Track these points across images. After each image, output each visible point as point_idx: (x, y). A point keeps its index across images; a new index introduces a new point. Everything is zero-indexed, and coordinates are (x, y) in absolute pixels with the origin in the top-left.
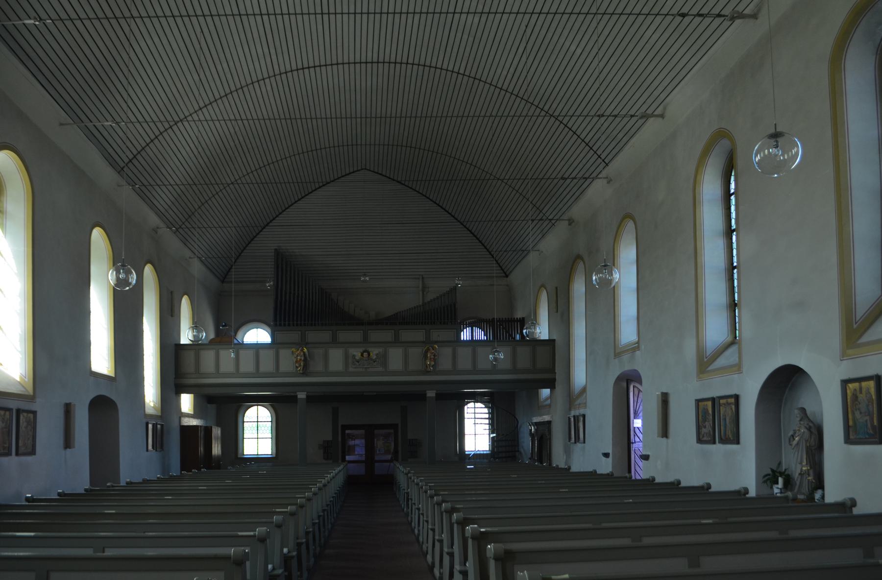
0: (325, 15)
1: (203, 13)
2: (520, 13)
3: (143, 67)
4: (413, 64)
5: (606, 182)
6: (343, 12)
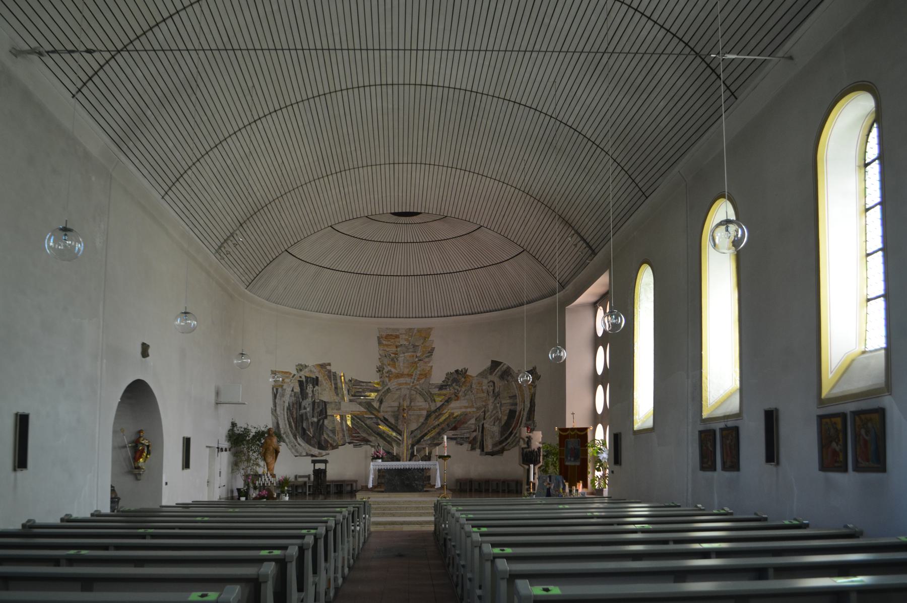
0: (414, 51)
1: (187, 48)
2: (542, 51)
3: (158, 57)
4: (164, 20)
5: (239, 487)
6: (410, 51)
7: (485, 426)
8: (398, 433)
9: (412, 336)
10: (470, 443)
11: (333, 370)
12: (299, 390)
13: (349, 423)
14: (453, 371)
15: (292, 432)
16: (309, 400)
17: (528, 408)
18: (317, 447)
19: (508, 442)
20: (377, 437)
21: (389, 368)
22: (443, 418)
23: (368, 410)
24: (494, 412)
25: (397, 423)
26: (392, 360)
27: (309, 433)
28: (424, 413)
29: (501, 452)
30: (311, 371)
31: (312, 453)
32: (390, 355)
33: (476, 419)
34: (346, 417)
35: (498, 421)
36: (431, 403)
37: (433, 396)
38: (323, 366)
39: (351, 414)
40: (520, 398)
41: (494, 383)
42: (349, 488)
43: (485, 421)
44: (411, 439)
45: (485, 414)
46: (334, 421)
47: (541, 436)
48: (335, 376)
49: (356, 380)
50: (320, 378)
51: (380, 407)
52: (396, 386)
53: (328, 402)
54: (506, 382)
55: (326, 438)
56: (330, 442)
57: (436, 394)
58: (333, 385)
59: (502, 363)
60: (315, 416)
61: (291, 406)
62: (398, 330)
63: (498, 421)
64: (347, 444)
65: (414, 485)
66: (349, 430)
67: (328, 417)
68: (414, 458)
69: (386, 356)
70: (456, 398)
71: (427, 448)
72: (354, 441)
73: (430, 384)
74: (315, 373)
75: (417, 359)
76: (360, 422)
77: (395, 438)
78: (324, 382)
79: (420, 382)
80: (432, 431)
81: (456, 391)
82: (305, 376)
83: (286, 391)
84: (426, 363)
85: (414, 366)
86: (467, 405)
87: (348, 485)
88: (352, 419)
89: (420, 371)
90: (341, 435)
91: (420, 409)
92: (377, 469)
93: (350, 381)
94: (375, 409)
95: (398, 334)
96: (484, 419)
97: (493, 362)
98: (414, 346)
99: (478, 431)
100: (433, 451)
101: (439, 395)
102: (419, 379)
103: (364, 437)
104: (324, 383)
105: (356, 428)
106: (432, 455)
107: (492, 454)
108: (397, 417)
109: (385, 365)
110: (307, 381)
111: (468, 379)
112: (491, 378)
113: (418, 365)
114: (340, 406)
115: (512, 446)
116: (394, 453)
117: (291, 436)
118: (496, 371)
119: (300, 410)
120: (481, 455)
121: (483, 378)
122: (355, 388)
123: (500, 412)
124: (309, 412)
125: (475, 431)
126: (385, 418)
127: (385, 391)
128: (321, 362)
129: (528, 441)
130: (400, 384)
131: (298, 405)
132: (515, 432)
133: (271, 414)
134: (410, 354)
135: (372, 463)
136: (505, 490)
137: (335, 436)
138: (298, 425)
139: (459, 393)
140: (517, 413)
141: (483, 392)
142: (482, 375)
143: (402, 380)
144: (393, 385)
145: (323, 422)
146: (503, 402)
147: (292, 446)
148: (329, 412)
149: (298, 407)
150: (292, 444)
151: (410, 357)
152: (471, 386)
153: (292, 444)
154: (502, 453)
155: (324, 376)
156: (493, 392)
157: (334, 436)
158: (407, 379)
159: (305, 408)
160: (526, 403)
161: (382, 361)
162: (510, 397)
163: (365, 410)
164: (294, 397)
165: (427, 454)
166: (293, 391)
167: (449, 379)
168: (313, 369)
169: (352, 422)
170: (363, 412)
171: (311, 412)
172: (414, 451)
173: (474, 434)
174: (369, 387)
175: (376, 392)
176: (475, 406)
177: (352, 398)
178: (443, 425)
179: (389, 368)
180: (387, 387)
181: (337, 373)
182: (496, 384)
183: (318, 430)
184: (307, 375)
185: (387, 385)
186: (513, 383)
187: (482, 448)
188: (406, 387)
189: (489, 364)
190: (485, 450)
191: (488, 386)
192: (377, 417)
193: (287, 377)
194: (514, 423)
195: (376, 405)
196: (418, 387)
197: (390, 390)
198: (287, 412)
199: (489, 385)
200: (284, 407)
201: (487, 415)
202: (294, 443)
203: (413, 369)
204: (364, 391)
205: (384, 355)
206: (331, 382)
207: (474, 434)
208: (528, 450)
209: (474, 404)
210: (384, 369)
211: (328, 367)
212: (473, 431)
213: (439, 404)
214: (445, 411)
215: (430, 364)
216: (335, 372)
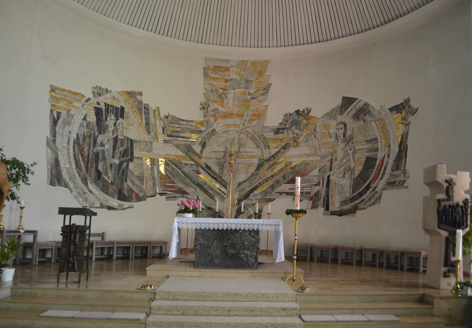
7: (332, 178)
8: (222, 184)
9: (244, 70)
10: (311, 199)
11: (145, 102)
12: (95, 120)
13: (162, 168)
14: (292, 111)
15: (80, 175)
16: (109, 135)
17: (395, 154)
18: (116, 196)
19: (362, 198)
20: (196, 189)
21: (216, 106)
22: (278, 168)
23: (187, 155)
24: (345, 161)
25: (222, 173)
26: (220, 96)
27: (107, 179)
28: (256, 161)
29: (353, 210)
30: (114, 98)
31: (108, 204)
32: (218, 90)
33: (319, 170)
34: (158, 162)
35: (350, 173)
36: (264, 150)
37: (267, 142)
38: (131, 94)
39: (165, 158)
40: (383, 141)
41: (345, 125)
42: (157, 251)
43: (331, 173)
44: (238, 193)
45: (331, 164)
46: (143, 164)
47: (469, 180)
48: (148, 109)
49: (175, 117)
50: (126, 109)
51: (202, 152)
52: (223, 128)
53: (136, 141)
54: (362, 123)
55: (131, 186)
56: (136, 191)
57: (270, 139)
58: (144, 120)
59: (357, 99)
60: (116, 156)
61: (81, 139)
62: (228, 61)
63: (350, 173)
64: (158, 195)
65: (242, 256)
66: (161, 178)
67: (135, 159)
68: (241, 216)
69: (212, 91)
70: (296, 144)
71: (257, 204)
72: (167, 192)
73: (264, 127)
74: (120, 101)
75: (249, 97)
76: (176, 168)
77: (218, 190)
78: (131, 114)
79: (253, 123)
80: (264, 183)
81: (295, 135)
82: (105, 104)
83: (75, 118)
84: (260, 101)
85: (246, 105)
86: (308, 152)
87: (154, 247)
88: (166, 164)
89: (253, 111)
90: (150, 183)
91: (251, 157)
92: (194, 228)
93: (167, 117)
94: (196, 154)
95: (228, 66)
96: (331, 170)
97: (344, 99)
98: (247, 81)
99: (321, 185)
100: (264, 208)
101: (275, 140)
102: (251, 121)
103: (180, 188)
104: (132, 116)
105: (171, 177)
106: (262, 213)
107: (340, 214)
108: (223, 166)
109: (211, 101)
110: (107, 110)
111: (311, 121)
112: (341, 118)
113: (251, 104)
114: (152, 147)
115: (369, 204)
116: (216, 209)
117: (79, 180)
118: (349, 110)
119: (94, 147)
120: (324, 214)
121: (331, 119)
122: (172, 126)
123: (352, 161)
124: (108, 150)
125: (318, 184)
126: (207, 166)
127: (209, 133)
128: (129, 90)
129: (448, 188)
130: (227, 126)
131: (92, 139)
132: (374, 185)
133: (46, 146)
134: (241, 90)
135: (176, 220)
136: (383, 264)
137: (143, 184)
138: (90, 165)
139: (299, 138)
140: (378, 162)
141: (330, 137)
142: (330, 115)
143: (230, 121)
144: (219, 126)
145: (128, 164)
146: (357, 148)
147: (79, 193)
148: (137, 153)
149: (92, 142)
150: (79, 190)
151: (241, 93)
152: (315, 130)
153: (79, 190)
154: (355, 212)
155: (132, 107)
156: (344, 135)
157: (141, 185)
158: (236, 120)
159: (102, 145)
160: (392, 147)
161: (208, 97)
162: (367, 141)
163: (183, 155)
164: (87, 128)
165: (257, 212)
166: (85, 119)
167: (287, 121)
168: (117, 96)
169: (165, 169)
170: (180, 156)
171: (112, 150)
172: (241, 208)
173: (317, 188)
174: (190, 127)
175: (199, 134)
176: (319, 154)
177: (167, 138)
178: (278, 177)
179: (216, 106)
180: (212, 129)
181: (150, 106)
182: (348, 126)
183: (120, 175)
184: (107, 103)
185: (212, 125)
186: (373, 123)
187: (327, 206)
188: (235, 129)
189: (339, 101)
190: (331, 209)
191: (338, 129)
192: (197, 164)
193: (78, 100)
194: (374, 173)
195: (197, 149)
196: (249, 130)
197: (215, 131)
198: (74, 147)
199: (338, 127)
200: (69, 139)
201: (334, 165)
202: (83, 190)
203: (244, 108)
204: (183, 131)
205: (210, 89)
206: (141, 115)
207: (317, 188)
208: (447, 203)
209: (318, 151)
210: (209, 106)
211: (139, 97)
212: (316, 185)
213: (274, 151)
214: (281, 160)
215: (265, 104)
216: (148, 105)
